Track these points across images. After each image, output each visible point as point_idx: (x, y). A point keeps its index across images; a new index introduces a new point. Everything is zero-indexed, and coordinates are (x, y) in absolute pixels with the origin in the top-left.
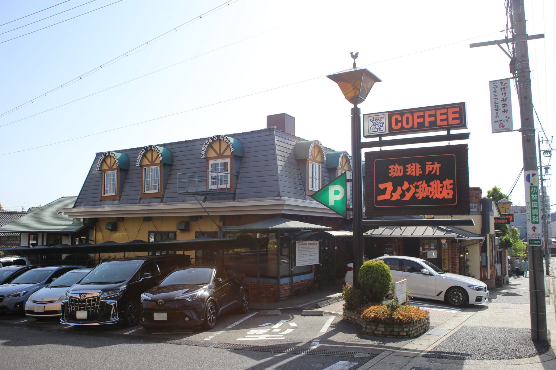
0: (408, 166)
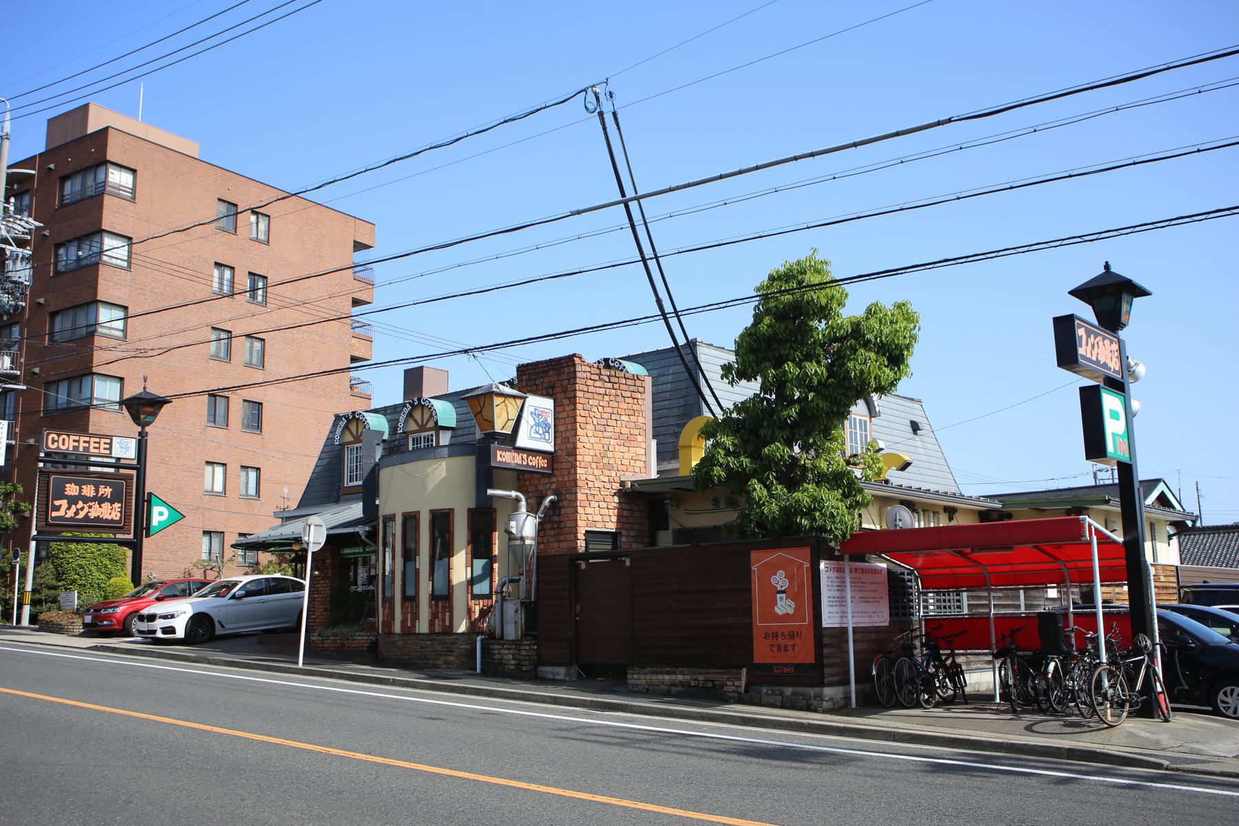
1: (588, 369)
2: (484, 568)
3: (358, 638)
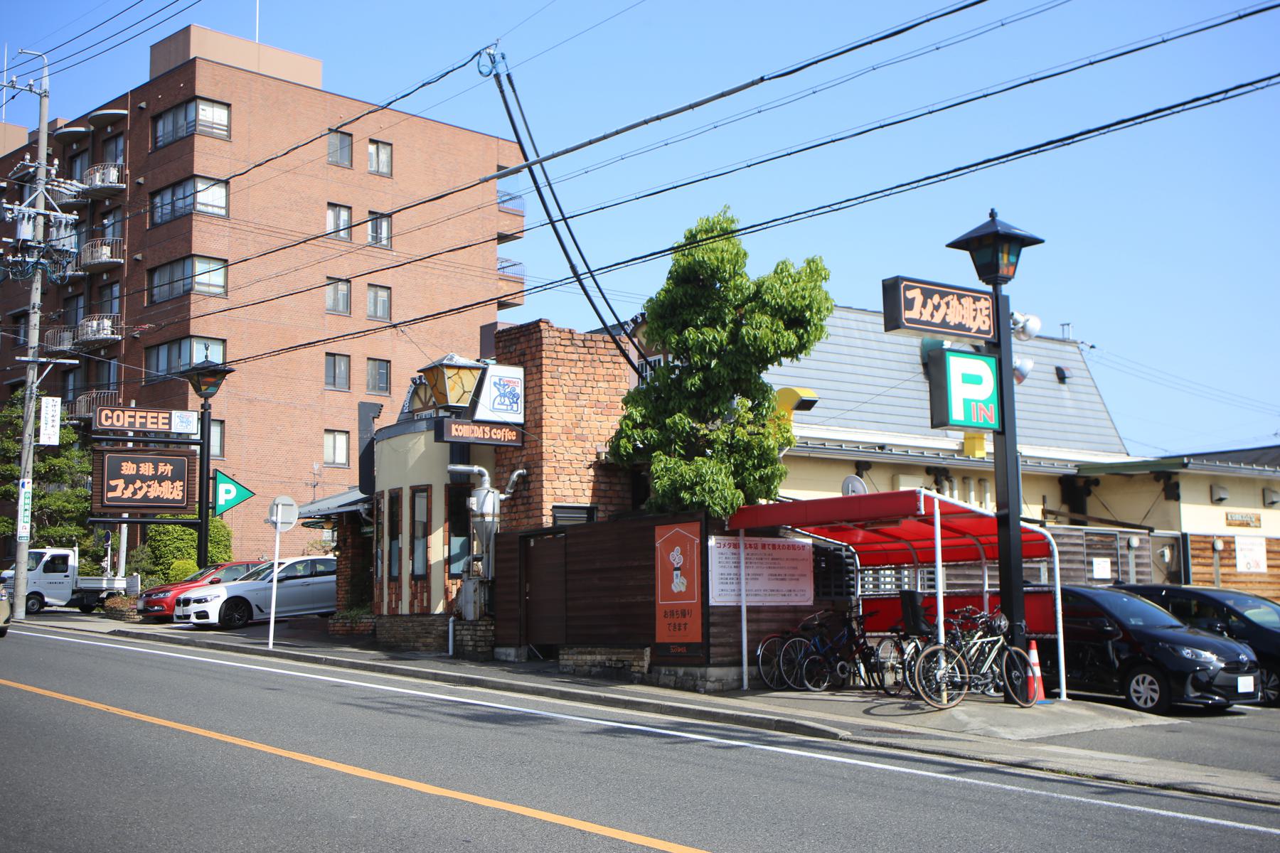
1: (557, 334)
2: (462, 546)
3: (366, 620)
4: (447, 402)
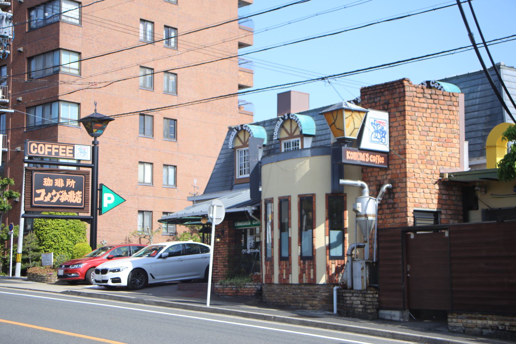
0: (56, 180)
1: (414, 89)
2: (338, 237)
4: (343, 134)
